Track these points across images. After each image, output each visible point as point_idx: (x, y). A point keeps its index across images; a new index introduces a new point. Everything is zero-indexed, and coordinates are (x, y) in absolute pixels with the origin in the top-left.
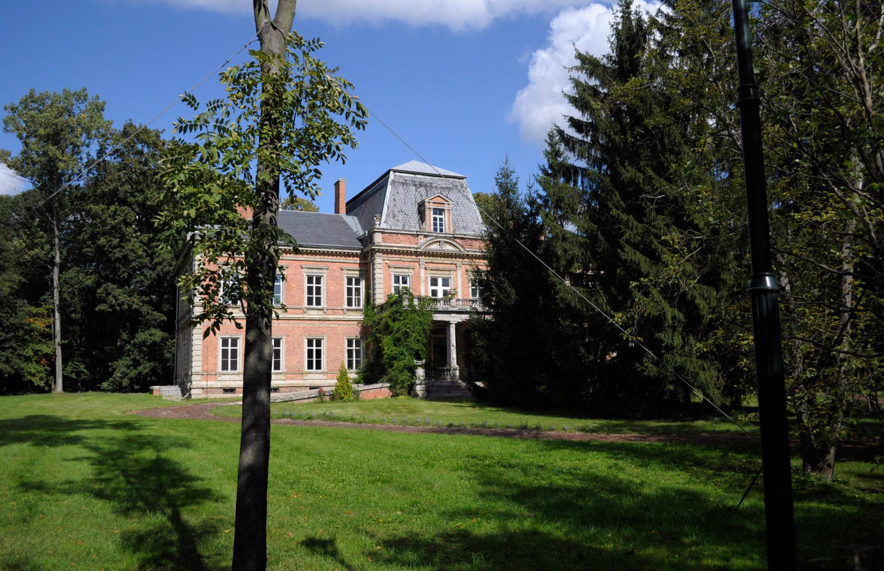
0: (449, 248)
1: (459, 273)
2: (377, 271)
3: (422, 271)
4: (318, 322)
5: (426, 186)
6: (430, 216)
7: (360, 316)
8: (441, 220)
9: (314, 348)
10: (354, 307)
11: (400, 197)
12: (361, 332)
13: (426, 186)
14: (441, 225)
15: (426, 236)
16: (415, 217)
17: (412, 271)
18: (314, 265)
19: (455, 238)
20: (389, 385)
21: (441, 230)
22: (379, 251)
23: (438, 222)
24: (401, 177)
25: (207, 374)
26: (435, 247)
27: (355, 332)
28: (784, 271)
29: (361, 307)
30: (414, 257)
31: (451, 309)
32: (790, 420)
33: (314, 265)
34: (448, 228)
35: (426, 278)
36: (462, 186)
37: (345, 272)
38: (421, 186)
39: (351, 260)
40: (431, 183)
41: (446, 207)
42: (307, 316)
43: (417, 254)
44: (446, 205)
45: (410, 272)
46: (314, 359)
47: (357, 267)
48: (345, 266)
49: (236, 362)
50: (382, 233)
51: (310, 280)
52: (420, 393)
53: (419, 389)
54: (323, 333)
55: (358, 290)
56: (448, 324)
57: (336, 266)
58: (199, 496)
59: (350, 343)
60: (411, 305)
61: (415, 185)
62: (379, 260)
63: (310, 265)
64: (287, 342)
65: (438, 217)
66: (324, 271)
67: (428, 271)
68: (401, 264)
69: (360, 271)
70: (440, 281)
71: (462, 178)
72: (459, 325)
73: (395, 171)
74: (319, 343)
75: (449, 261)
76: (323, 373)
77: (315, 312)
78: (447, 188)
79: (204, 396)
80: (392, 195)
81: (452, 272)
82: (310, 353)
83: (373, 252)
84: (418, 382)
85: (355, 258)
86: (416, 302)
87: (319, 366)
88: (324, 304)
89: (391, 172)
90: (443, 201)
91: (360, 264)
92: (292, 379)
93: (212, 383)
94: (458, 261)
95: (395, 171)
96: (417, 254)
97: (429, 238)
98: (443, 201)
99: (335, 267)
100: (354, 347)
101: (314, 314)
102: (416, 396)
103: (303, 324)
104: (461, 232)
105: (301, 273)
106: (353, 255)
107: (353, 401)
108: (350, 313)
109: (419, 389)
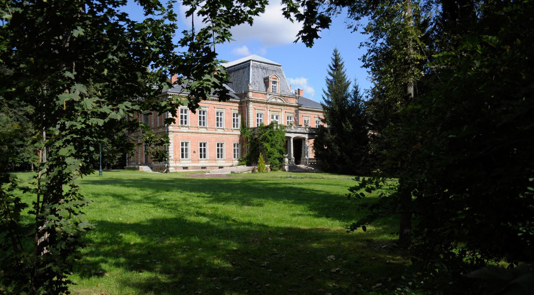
0: (279, 101)
2: (250, 111)
3: (268, 111)
6: (271, 84)
10: (236, 128)
11: (255, 74)
13: (266, 69)
15: (270, 95)
16: (263, 85)
18: (220, 107)
22: (252, 101)
25: (176, 160)
26: (274, 100)
27: (237, 140)
28: (30, 57)
29: (239, 128)
31: (291, 131)
32: (227, 259)
33: (220, 107)
34: (278, 91)
38: (264, 69)
41: (277, 81)
42: (217, 132)
43: (267, 103)
45: (263, 112)
48: (232, 108)
52: (287, 169)
53: (286, 168)
54: (224, 140)
56: (290, 138)
57: (229, 108)
58: (144, 227)
59: (234, 145)
60: (277, 129)
62: (251, 105)
63: (218, 106)
65: (274, 85)
68: (259, 108)
70: (275, 117)
73: (253, 61)
77: (220, 130)
79: (175, 171)
83: (248, 101)
86: (279, 128)
87: (205, 157)
88: (189, 124)
91: (239, 107)
93: (178, 165)
94: (282, 107)
95: (253, 61)
96: (267, 103)
98: (276, 77)
102: (285, 170)
104: (283, 94)
106: (236, 102)
108: (235, 131)
109: (286, 168)
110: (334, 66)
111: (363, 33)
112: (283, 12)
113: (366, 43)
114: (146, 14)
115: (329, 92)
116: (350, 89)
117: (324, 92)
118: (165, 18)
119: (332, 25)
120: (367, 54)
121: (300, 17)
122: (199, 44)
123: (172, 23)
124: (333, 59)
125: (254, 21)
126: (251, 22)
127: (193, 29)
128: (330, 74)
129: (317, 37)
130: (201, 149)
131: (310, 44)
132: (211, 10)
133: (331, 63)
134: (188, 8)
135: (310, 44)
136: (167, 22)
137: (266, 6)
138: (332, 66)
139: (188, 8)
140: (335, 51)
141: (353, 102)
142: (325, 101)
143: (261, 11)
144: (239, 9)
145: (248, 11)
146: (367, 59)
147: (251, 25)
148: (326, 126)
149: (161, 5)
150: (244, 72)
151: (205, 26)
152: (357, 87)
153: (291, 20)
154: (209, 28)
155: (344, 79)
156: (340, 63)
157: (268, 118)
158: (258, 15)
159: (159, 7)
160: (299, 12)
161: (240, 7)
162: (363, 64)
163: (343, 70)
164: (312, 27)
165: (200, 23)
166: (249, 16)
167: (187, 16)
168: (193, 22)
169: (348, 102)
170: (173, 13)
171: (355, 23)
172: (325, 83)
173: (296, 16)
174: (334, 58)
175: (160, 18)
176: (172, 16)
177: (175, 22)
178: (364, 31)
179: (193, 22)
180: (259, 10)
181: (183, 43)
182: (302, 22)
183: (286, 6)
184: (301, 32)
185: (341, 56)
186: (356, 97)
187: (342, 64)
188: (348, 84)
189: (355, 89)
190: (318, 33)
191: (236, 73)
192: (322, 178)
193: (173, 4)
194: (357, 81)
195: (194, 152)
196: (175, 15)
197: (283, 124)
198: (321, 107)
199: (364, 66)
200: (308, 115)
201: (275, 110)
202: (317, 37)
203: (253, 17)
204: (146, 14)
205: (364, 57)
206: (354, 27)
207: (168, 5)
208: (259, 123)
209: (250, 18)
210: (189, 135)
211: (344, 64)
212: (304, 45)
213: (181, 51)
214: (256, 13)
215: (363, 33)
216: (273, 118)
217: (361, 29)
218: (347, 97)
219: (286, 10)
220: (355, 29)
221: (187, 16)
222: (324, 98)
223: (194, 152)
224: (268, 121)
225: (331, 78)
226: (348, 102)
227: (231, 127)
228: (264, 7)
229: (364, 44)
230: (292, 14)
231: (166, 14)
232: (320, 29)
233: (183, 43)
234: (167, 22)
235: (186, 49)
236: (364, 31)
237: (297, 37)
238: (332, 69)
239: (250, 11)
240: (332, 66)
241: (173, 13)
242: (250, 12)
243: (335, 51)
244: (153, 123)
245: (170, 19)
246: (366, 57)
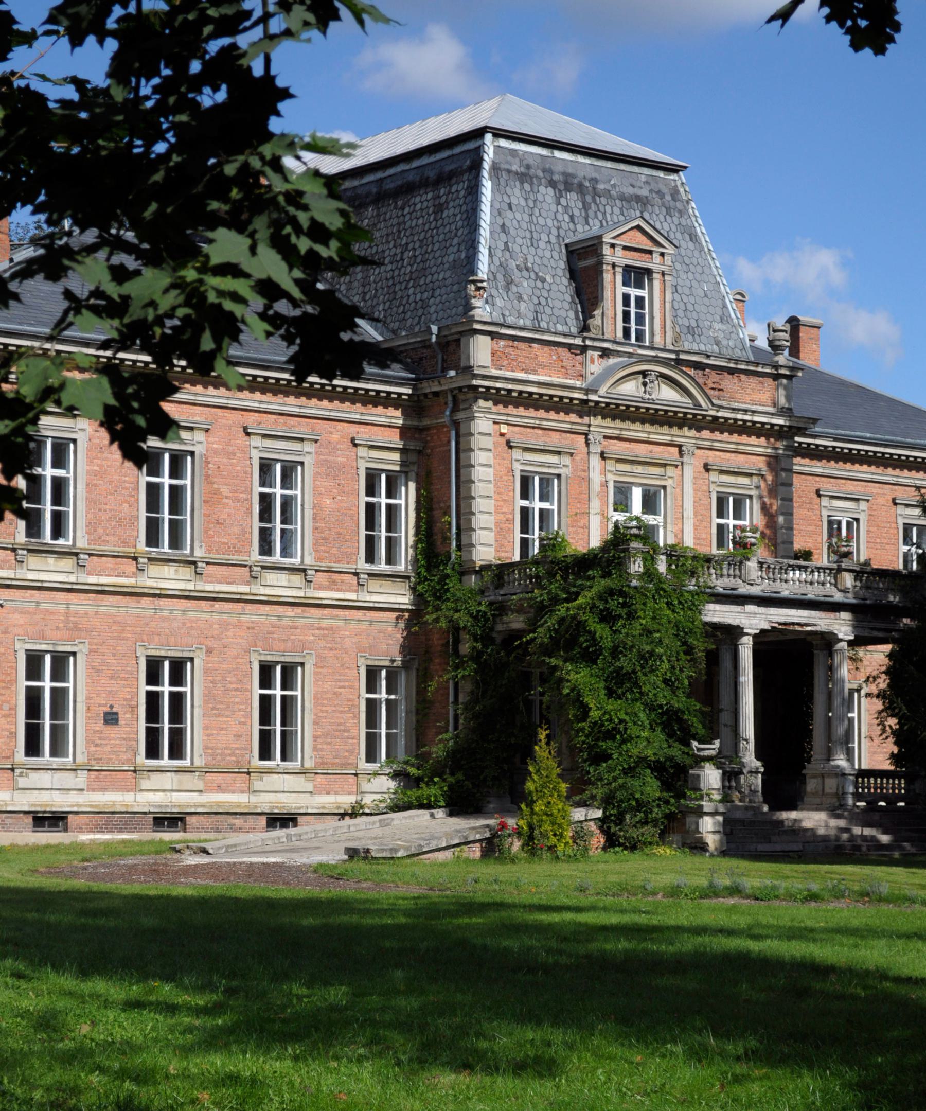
0: (667, 395)
1: (689, 472)
2: (480, 457)
3: (595, 461)
4: (290, 611)
6: (614, 288)
7: (403, 598)
8: (640, 301)
9: (166, 689)
10: (382, 566)
12: (403, 647)
13: (581, 189)
14: (640, 319)
17: (567, 460)
19: (679, 362)
20: (599, 814)
21: (640, 336)
23: (633, 310)
24: (513, 153)
26: (631, 389)
27: (386, 642)
30: (573, 418)
31: (744, 589)
34: (660, 331)
35: (605, 484)
36: (675, 193)
37: (362, 452)
39: (380, 414)
40: (594, 181)
41: (655, 263)
43: (585, 408)
44: (657, 258)
46: (166, 725)
47: (394, 438)
48: (364, 434)
50: (493, 335)
52: (712, 841)
54: (304, 646)
55: (392, 511)
57: (338, 434)
59: (372, 674)
60: (649, 574)
61: (552, 184)
62: (485, 422)
63: (270, 424)
64: (206, 671)
65: (634, 292)
66: (308, 447)
67: (610, 465)
69: (403, 451)
70: (637, 495)
71: (676, 171)
72: (763, 640)
74: (289, 672)
75: (662, 434)
76: (303, 772)
77: (282, 578)
78: (638, 198)
80: (497, 212)
81: (670, 471)
82: (33, 700)
83: (466, 396)
84: (707, 806)
85: (391, 412)
86: (662, 566)
87: (176, 751)
88: (78, 535)
89: (488, 137)
90: (647, 245)
91: (404, 431)
92: (220, 789)
95: (499, 134)
96: (585, 408)
97: (612, 361)
98: (647, 245)
99: (335, 437)
100: (383, 695)
101: (280, 585)
102: (699, 847)
105: (245, 451)
108: (374, 585)
150: (439, 208)
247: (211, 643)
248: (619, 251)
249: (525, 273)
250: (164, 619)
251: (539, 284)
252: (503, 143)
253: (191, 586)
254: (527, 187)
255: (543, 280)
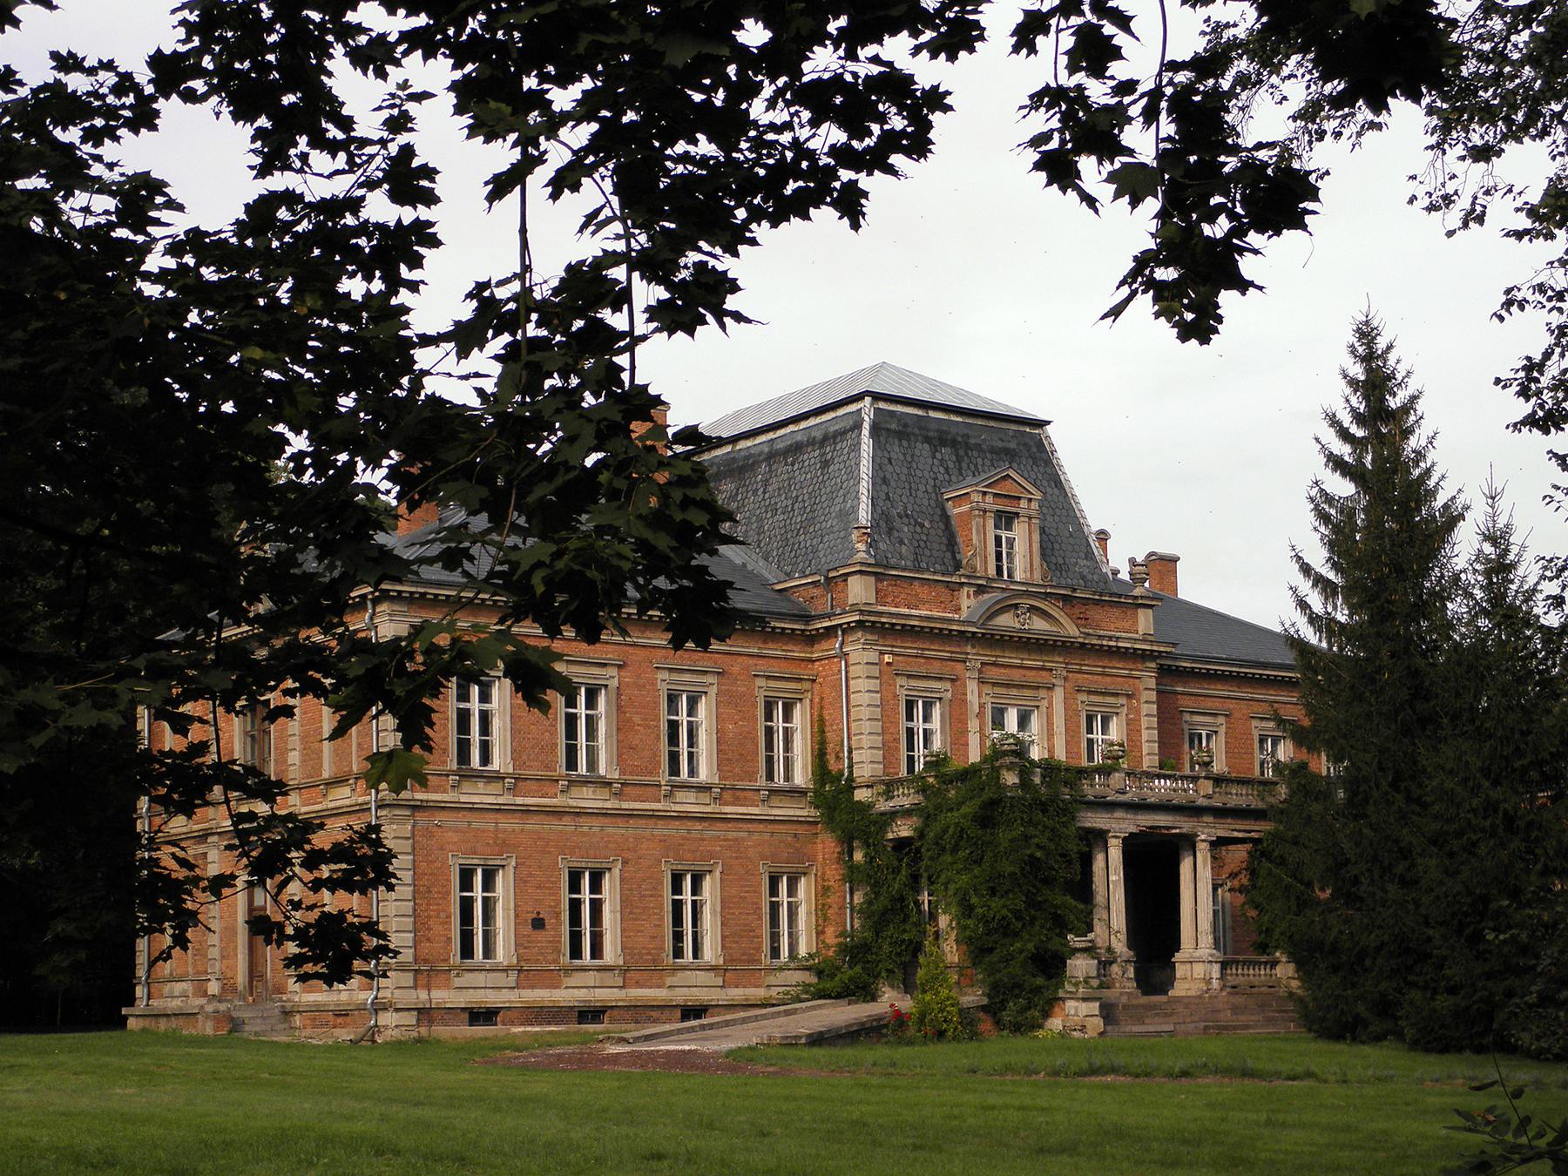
3: (972, 687)
5: (954, 443)
13: (954, 443)
17: (948, 685)
26: (1006, 621)
35: (982, 706)
44: (1024, 504)
49: (571, 925)
51: (673, 699)
61: (927, 440)
65: (1004, 534)
77: (691, 796)
78: (1007, 451)
81: (1043, 693)
93: (441, 996)
94: (1056, 662)
103: (661, 829)
107: (968, 1025)
110: (1359, 418)
111: (1519, 235)
112: (1033, 156)
113: (1541, 288)
114: (263, 171)
115: (1336, 567)
116: (1464, 549)
117: (1306, 569)
118: (371, 185)
119: (1325, 215)
120: (1547, 355)
121: (1132, 184)
122: (563, 331)
123: (408, 215)
124: (1353, 383)
125: (869, 206)
126: (851, 205)
127: (526, 268)
128: (1336, 463)
129: (1243, 285)
130: (575, 906)
131: (1201, 327)
132: (629, 158)
133: (1341, 400)
134: (504, 154)
135: (1201, 327)
136: (380, 209)
137: (936, 118)
138: (1346, 419)
139: (504, 154)
140: (1366, 333)
141: (1483, 623)
142: (1313, 619)
143: (908, 152)
144: (786, 138)
145: (834, 151)
146: (1545, 381)
147: (855, 226)
148: (1323, 765)
149: (346, 124)
150: (826, 464)
151: (589, 248)
152: (1507, 531)
153: (1090, 201)
154: (611, 258)
155: (1419, 491)
156: (1394, 403)
157: (973, 725)
158: (891, 171)
159: (334, 132)
160: (1130, 152)
161: (788, 126)
162: (1524, 408)
163: (1413, 442)
164: (1207, 230)
165: (566, 231)
166: (846, 175)
167: (493, 197)
168: (523, 231)
169: (1450, 626)
170: (415, 163)
171: (1473, 176)
172: (1310, 518)
173: (1111, 178)
174: (1358, 371)
175: (341, 186)
176: (408, 180)
177: (423, 213)
178: (1524, 223)
179: (523, 231)
180: (891, 142)
181: (465, 337)
182: (1152, 205)
183: (1055, 123)
184: (1143, 262)
185: (1402, 359)
186: (1497, 596)
187: (1407, 408)
188: (1452, 519)
189: (1488, 549)
190: (1247, 266)
191: (781, 468)
192: (1309, 1075)
193: (411, 107)
194: (1503, 504)
195: (538, 924)
196: (429, 172)
197: (1061, 755)
198: (1289, 657)
199: (1531, 421)
200: (1209, 704)
201: (1016, 675)
202: (1243, 285)
203: (864, 182)
204: (263, 171)
205: (1532, 368)
206: (1463, 203)
207: (386, 114)
208: (920, 750)
209: (853, 184)
210: (508, 824)
211: (1421, 406)
212: (1165, 331)
213: (458, 380)
214: (876, 161)
215: (1519, 235)
216: (998, 723)
217: (1504, 214)
218: (1442, 596)
219: (1054, 144)
220: (1475, 216)
221: (493, 197)
222: (1303, 605)
223: (538, 924)
224: (974, 740)
225: (1343, 488)
226: (1450, 626)
227: (752, 776)
228: (929, 126)
229: (1526, 293)
230: (1087, 165)
231: (377, 168)
232: (1253, 238)
233: (465, 337)
234: (380, 209)
235: (486, 361)
236: (1524, 223)
237: (1125, 290)
238: (1345, 435)
239: (847, 147)
240: (1346, 419)
241: (415, 163)
242: (843, 155)
243: (1366, 333)
244: (294, 757)
245: (398, 197)
246: (1540, 367)
247: (627, 855)
248: (989, 499)
249: (905, 520)
250: (584, 834)
251: (918, 529)
252: (882, 405)
253: (608, 805)
254: (905, 443)
255: (922, 526)
